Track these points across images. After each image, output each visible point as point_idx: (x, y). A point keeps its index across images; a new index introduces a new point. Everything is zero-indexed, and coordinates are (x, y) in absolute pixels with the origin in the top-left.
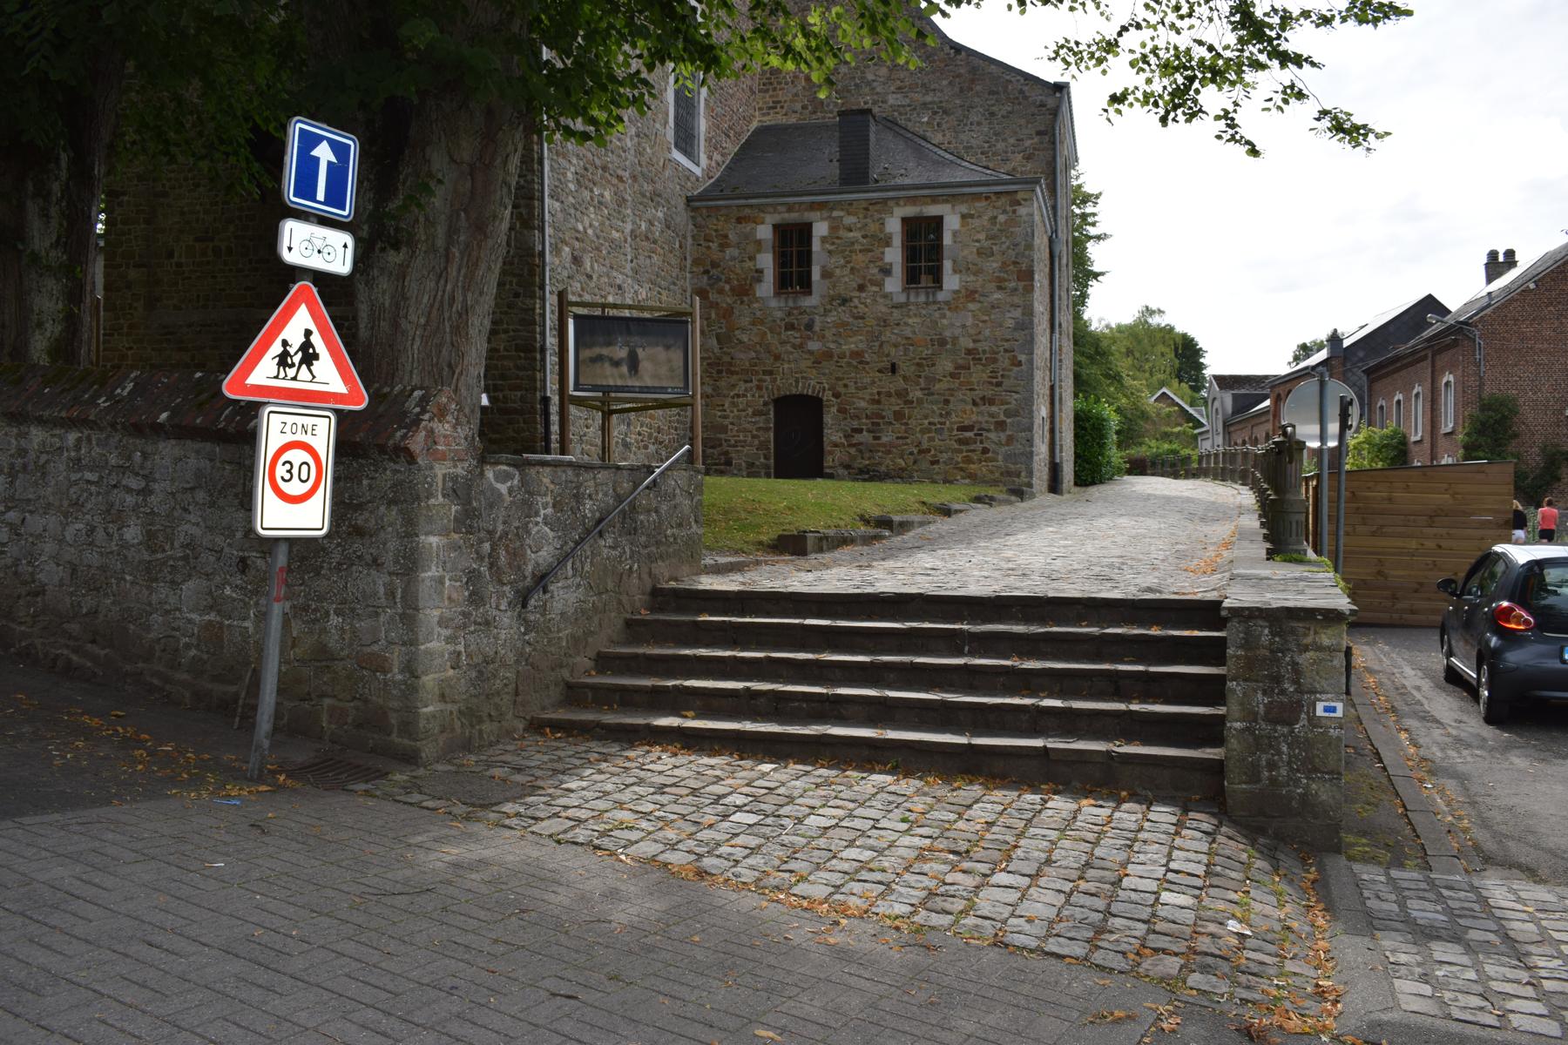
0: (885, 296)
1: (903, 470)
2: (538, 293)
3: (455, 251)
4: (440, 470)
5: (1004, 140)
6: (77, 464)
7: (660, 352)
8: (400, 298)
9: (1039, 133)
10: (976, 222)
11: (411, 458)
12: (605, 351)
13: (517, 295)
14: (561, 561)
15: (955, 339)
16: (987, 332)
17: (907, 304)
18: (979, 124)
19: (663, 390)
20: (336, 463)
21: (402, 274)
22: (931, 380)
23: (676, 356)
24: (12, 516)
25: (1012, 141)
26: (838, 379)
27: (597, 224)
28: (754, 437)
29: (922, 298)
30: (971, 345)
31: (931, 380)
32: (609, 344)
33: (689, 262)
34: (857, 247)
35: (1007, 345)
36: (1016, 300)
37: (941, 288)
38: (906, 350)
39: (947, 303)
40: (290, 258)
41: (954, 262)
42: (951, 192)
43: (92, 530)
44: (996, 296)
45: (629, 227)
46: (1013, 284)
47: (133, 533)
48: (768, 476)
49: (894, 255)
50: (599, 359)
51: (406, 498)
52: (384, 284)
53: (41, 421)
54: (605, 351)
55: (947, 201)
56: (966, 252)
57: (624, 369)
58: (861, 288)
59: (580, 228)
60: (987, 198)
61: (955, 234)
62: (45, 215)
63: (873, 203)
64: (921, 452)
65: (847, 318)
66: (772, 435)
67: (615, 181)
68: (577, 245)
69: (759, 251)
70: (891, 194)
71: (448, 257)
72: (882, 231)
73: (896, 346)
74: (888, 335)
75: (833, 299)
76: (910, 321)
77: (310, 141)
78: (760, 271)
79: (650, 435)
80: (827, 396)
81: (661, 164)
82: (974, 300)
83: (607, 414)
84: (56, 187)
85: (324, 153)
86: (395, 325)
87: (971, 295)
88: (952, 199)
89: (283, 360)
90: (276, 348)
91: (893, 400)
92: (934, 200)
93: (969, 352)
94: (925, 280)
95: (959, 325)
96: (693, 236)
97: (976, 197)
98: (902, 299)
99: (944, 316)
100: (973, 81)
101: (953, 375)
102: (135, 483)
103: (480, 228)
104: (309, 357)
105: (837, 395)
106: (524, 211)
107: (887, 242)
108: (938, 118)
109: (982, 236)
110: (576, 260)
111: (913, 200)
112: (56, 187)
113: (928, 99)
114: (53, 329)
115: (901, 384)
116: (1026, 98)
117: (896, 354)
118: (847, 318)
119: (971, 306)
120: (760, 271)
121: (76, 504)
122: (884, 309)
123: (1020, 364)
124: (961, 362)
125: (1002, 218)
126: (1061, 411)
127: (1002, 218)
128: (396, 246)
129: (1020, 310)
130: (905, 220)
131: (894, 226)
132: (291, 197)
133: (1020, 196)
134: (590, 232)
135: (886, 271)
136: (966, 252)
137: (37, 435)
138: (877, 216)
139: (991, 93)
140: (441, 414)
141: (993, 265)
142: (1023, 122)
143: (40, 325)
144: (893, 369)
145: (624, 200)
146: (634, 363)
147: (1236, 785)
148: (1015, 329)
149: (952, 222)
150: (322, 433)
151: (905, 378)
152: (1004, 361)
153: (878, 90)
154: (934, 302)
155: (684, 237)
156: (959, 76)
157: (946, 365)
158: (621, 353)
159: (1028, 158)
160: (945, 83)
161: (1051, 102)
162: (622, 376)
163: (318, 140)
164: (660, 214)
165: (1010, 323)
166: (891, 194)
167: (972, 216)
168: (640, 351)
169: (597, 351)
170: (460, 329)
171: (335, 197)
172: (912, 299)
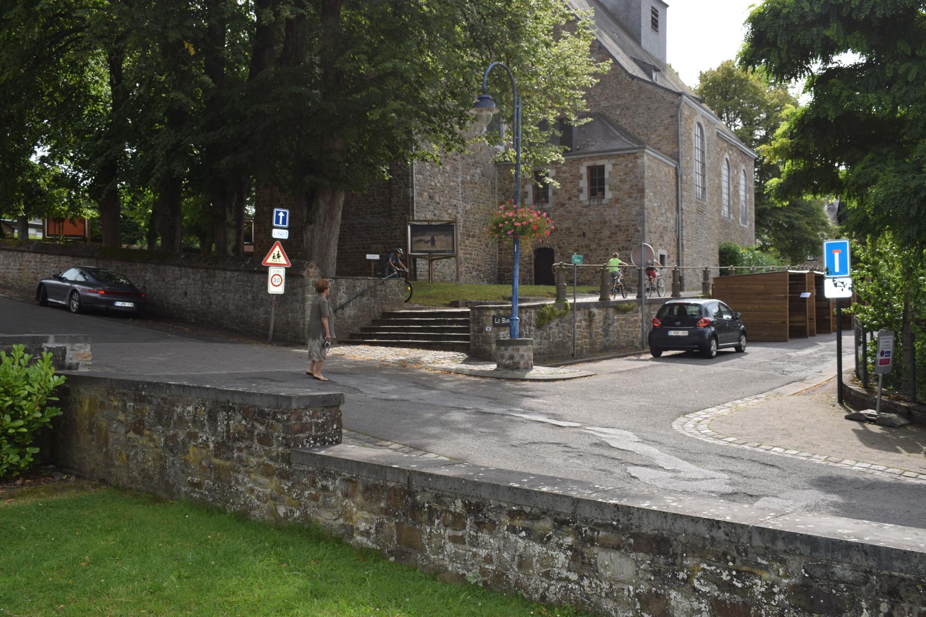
0: (580, 202)
1: (589, 281)
2: (411, 212)
3: (326, 224)
4: (311, 280)
5: (655, 121)
6: (237, 280)
7: (443, 237)
8: (313, 236)
9: (671, 117)
10: (619, 167)
11: (304, 278)
12: (422, 238)
13: (403, 214)
14: (348, 302)
15: (610, 220)
16: (624, 217)
17: (589, 206)
18: (643, 114)
19: (444, 251)
20: (286, 279)
21: (313, 231)
22: (600, 240)
23: (449, 239)
24: (223, 294)
25: (658, 121)
26: (560, 240)
27: (441, 181)
28: (525, 267)
29: (596, 203)
30: (617, 223)
31: (600, 240)
32: (423, 235)
33: (497, 189)
34: (568, 180)
35: (633, 223)
36: (637, 202)
37: (604, 198)
38: (589, 227)
39: (607, 204)
40: (274, 236)
41: (610, 186)
42: (607, 154)
43: (241, 296)
44: (628, 200)
45: (460, 179)
46: (635, 195)
47: (250, 297)
48: (531, 284)
49: (584, 184)
50: (420, 241)
51: (303, 286)
52: (309, 233)
53: (230, 270)
54: (422, 238)
55: (606, 158)
56: (615, 181)
57: (429, 244)
58: (570, 199)
59: (433, 184)
60: (624, 156)
61: (610, 173)
62: (231, 212)
63: (574, 160)
64: (596, 272)
65: (563, 212)
66: (533, 266)
67: (453, 161)
68: (431, 191)
69: (526, 184)
70: (582, 156)
71: (324, 226)
72: (578, 172)
73: (585, 224)
74: (582, 220)
75: (558, 204)
76: (591, 213)
77: (278, 212)
78: (526, 193)
79: (473, 268)
80: (556, 248)
81: (479, 149)
82: (618, 203)
83: (431, 261)
84: (234, 204)
85: (281, 215)
86: (311, 244)
87: (617, 200)
88: (608, 157)
89: (274, 257)
90: (272, 255)
91: (584, 249)
92: (601, 158)
93: (617, 226)
94: (599, 194)
95: (612, 214)
96: (499, 179)
97: (619, 156)
98: (587, 203)
99: (605, 211)
100: (640, 93)
101: (609, 237)
102: (250, 285)
103: (332, 218)
104: (279, 257)
105: (560, 248)
106: (405, 181)
107: (581, 178)
108: (624, 111)
109: (622, 174)
110: (431, 197)
111: (591, 158)
112: (234, 204)
113: (619, 103)
114: (233, 243)
115: (587, 242)
116: (665, 100)
117: (585, 228)
118: (563, 212)
119: (617, 205)
120: (526, 193)
121: (238, 290)
122: (580, 208)
123: (639, 231)
124: (613, 231)
125: (630, 165)
126: (683, 251)
127: (630, 165)
128: (311, 224)
129: (638, 207)
130: (588, 167)
131: (583, 170)
132: (275, 224)
133: (638, 155)
134: (438, 185)
135: (581, 191)
136: (615, 181)
137: (229, 274)
138: (576, 166)
139: (649, 98)
140: (311, 267)
141: (626, 187)
142: (664, 112)
143: (230, 242)
144: (584, 235)
145: (457, 168)
146: (433, 242)
147: (472, 347)
148: (637, 215)
149: (608, 168)
150: (282, 272)
151: (589, 239)
152: (632, 230)
153: (597, 99)
154: (601, 204)
155: (494, 179)
156: (633, 91)
157: (607, 233)
158: (429, 238)
159: (666, 129)
160: (627, 94)
161: (676, 101)
162: (428, 247)
163: (279, 212)
164: (478, 171)
165: (634, 213)
166: (582, 156)
167: (617, 165)
168: (435, 237)
169: (419, 238)
170: (328, 244)
171: (284, 223)
172: (592, 203)
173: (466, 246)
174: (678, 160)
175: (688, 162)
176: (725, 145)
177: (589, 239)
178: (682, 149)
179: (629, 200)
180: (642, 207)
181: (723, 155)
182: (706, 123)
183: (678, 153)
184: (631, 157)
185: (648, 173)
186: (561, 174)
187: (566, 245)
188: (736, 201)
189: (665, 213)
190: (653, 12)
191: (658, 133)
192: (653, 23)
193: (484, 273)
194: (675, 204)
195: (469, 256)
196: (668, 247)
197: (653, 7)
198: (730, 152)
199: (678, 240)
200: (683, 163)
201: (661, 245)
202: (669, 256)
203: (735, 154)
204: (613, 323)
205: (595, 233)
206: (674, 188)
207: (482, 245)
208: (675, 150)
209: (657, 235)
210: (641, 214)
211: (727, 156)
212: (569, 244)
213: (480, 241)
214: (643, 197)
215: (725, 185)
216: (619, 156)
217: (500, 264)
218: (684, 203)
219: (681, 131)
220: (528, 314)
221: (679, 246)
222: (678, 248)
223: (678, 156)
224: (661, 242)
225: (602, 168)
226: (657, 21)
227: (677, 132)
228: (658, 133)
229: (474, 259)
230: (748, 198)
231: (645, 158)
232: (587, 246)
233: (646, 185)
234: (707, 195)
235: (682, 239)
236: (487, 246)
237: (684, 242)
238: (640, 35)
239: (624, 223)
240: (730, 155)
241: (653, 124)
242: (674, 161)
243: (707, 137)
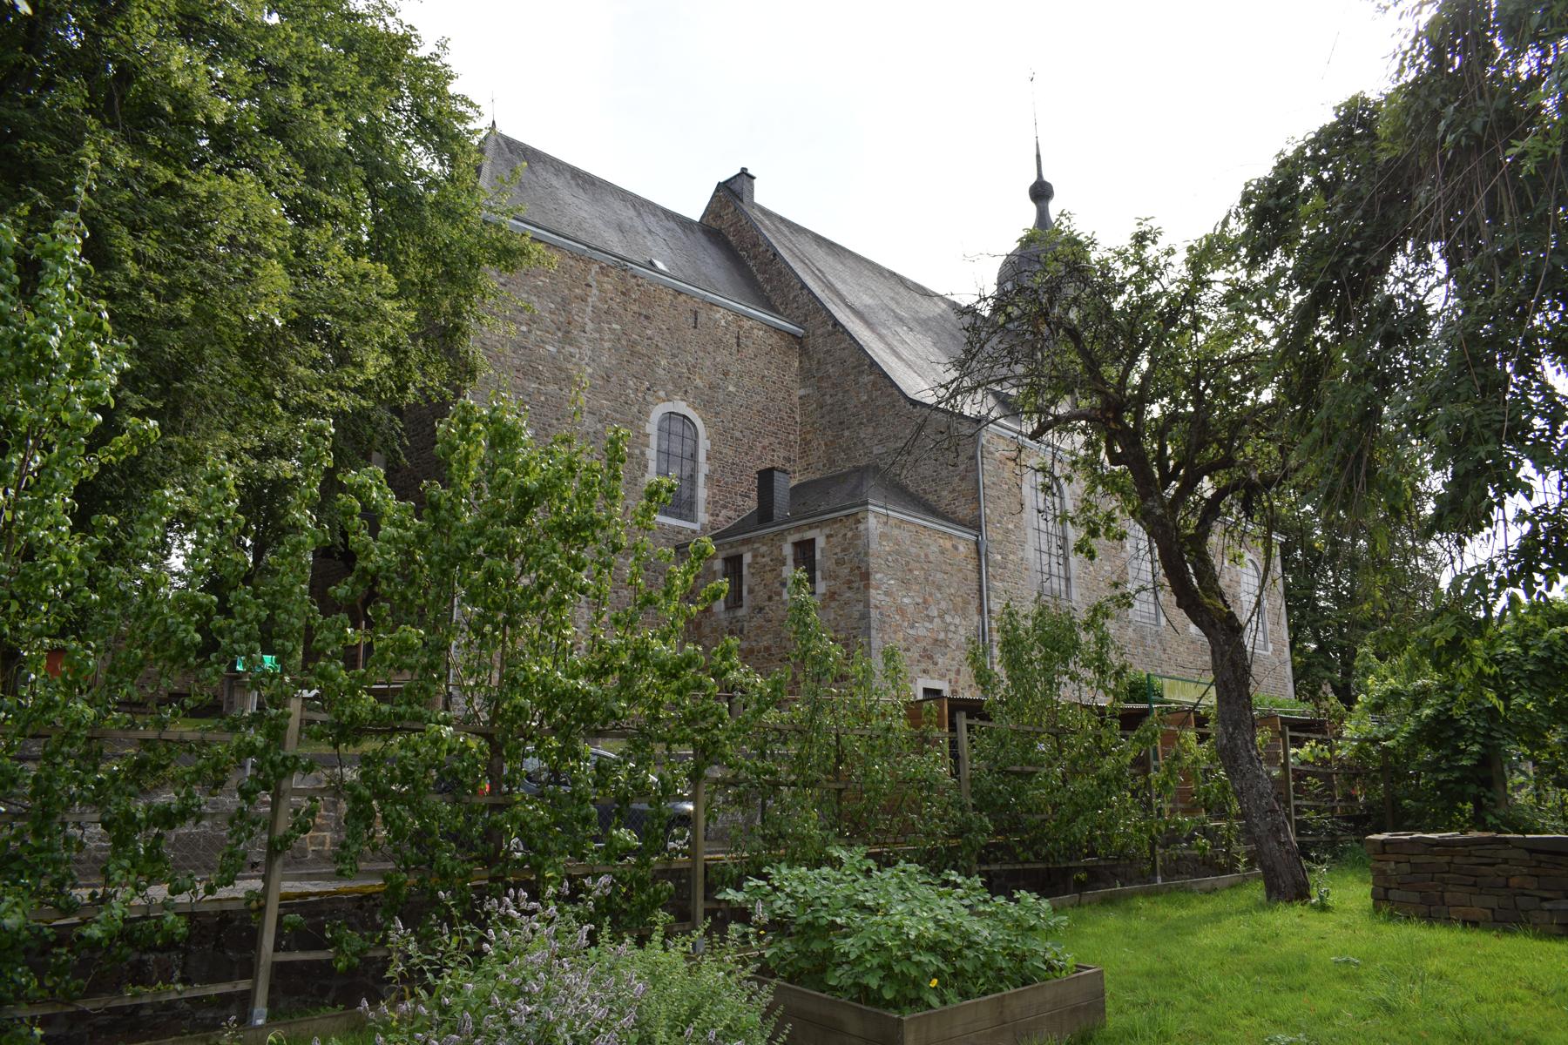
34: (768, 568)
61: (822, 550)
92: (810, 527)
97: (835, 520)
109: (838, 550)
127: (850, 534)
133: (860, 516)
149: (821, 542)
159: (962, 479)
167: (831, 536)
208: (976, 513)
216: (835, 520)
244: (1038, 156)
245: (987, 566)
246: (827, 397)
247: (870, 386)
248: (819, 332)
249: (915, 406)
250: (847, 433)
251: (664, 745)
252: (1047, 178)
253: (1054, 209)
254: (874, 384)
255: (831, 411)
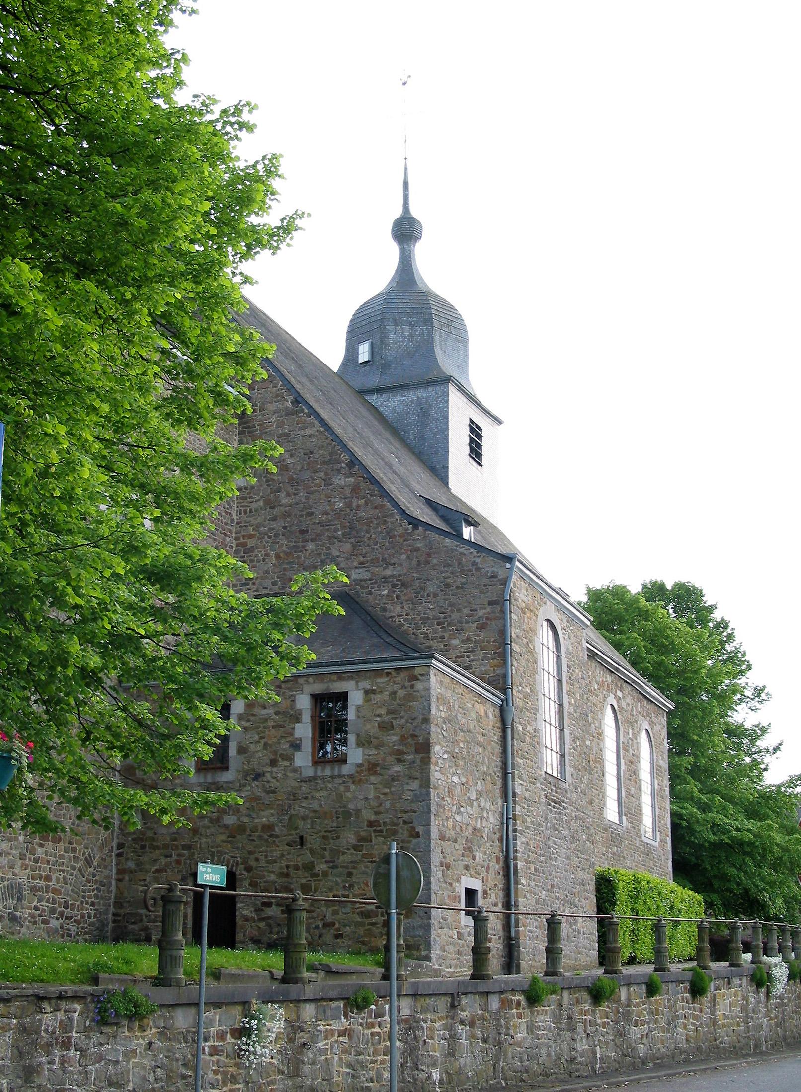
0: (295, 770)
5: (459, 611)
10: (378, 697)
15: (358, 811)
17: (314, 778)
22: (336, 853)
26: (250, 853)
30: (373, 818)
31: (336, 853)
34: (271, 723)
35: (406, 817)
39: (351, 776)
41: (358, 736)
49: (304, 730)
55: (352, 678)
58: (273, 763)
60: (388, 674)
61: (358, 708)
65: (259, 792)
75: (246, 774)
79: (53, 911)
87: (372, 767)
88: (356, 676)
91: (300, 872)
92: (340, 676)
93: (371, 824)
97: (378, 673)
98: (309, 772)
101: (356, 848)
105: (249, 869)
109: (383, 711)
113: (388, 572)
115: (308, 857)
116: (478, 569)
117: (304, 827)
119: (373, 778)
123: (418, 835)
124: (363, 834)
126: (517, 883)
127: (401, 693)
133: (417, 671)
135: (296, 746)
136: (368, 726)
149: (356, 698)
151: (312, 851)
159: (481, 627)
160: (404, 557)
165: (408, 796)
167: (373, 692)
173: (36, 861)
174: (504, 690)
175: (526, 697)
176: (609, 679)
177: (312, 851)
178: (516, 668)
179: (397, 768)
180: (426, 783)
181: (605, 698)
182: (565, 623)
183: (505, 676)
184: (401, 677)
185: (437, 712)
186: (257, 710)
187: (263, 863)
188: (633, 790)
189: (477, 800)
190: (472, 430)
191: (464, 635)
192: (472, 450)
193: (77, 922)
194: (499, 783)
195: (42, 883)
196: (484, 874)
197: (471, 421)
198: (619, 694)
199: (507, 857)
200: (517, 696)
201: (467, 867)
202: (485, 893)
203: (629, 700)
204: (314, 1038)
205: (324, 837)
206: (498, 749)
207: (76, 859)
208: (499, 671)
209: (459, 846)
210: (423, 796)
211: (611, 700)
212: (268, 862)
213: (74, 850)
214: (426, 761)
215: (610, 757)
216: (378, 673)
217: (118, 904)
218: (518, 781)
219: (514, 632)
220: (60, 1015)
221: (508, 872)
222: (507, 876)
223: (505, 683)
224: (468, 860)
225: (343, 697)
226: (479, 446)
227: (503, 632)
228: (464, 635)
229: (55, 891)
230: (656, 786)
231: (433, 679)
232: (309, 867)
233: (433, 735)
234: (569, 770)
235: (515, 858)
236: (88, 862)
237: (520, 864)
238: (446, 468)
239: (384, 818)
240: (618, 699)
241: (455, 616)
242: (498, 693)
243: (568, 652)
244: (406, 169)
245: (513, 739)
246: (283, 495)
247: (348, 491)
248: (272, 407)
249: (416, 527)
250: (311, 546)
251: (693, 953)
252: (415, 212)
253: (421, 252)
254: (355, 489)
255: (286, 515)
